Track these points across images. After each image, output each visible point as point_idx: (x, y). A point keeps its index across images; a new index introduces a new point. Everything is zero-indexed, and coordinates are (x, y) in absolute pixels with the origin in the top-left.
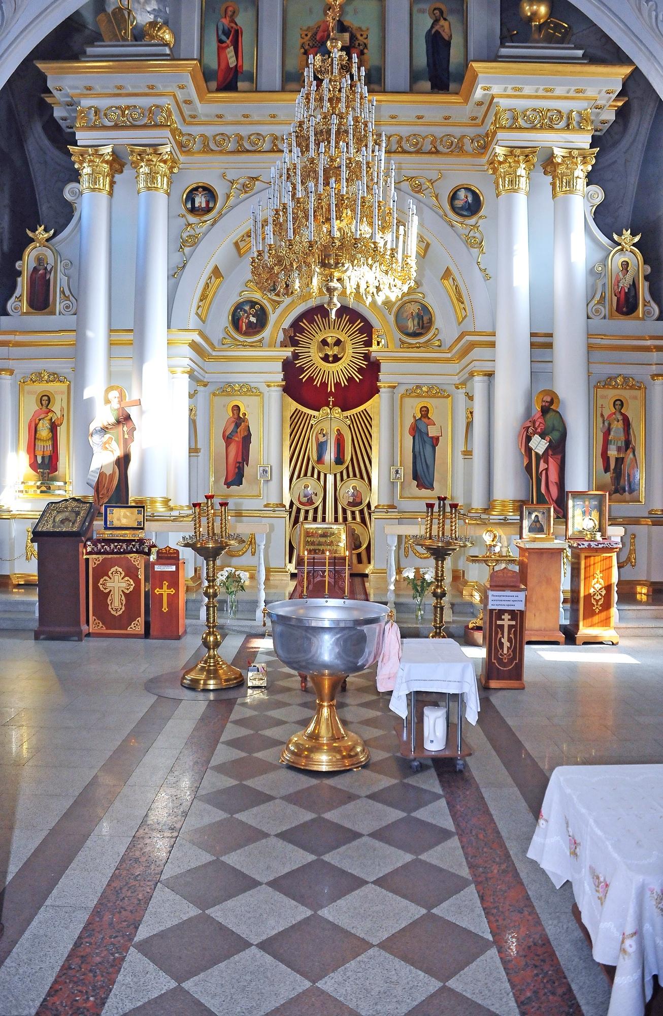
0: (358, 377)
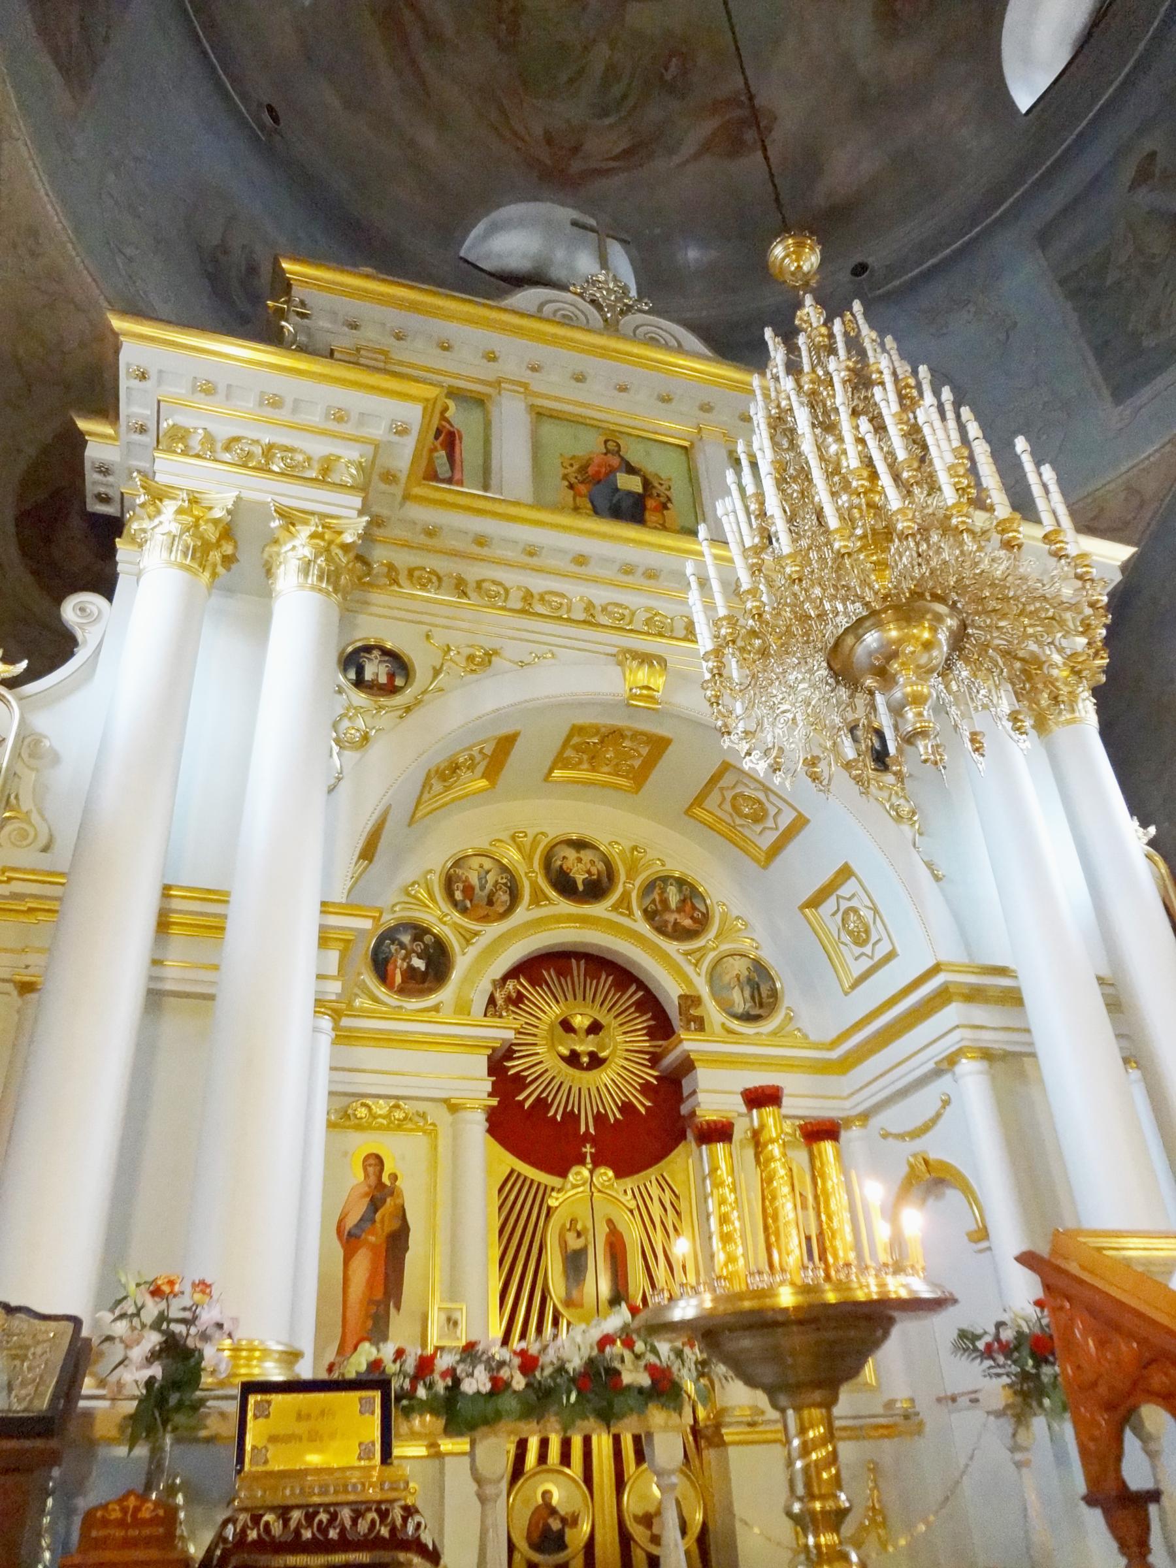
0: (642, 1104)
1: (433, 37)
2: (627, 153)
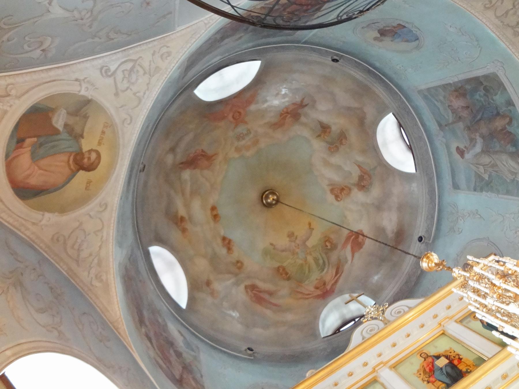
1: (271, 294)
2: (337, 273)
